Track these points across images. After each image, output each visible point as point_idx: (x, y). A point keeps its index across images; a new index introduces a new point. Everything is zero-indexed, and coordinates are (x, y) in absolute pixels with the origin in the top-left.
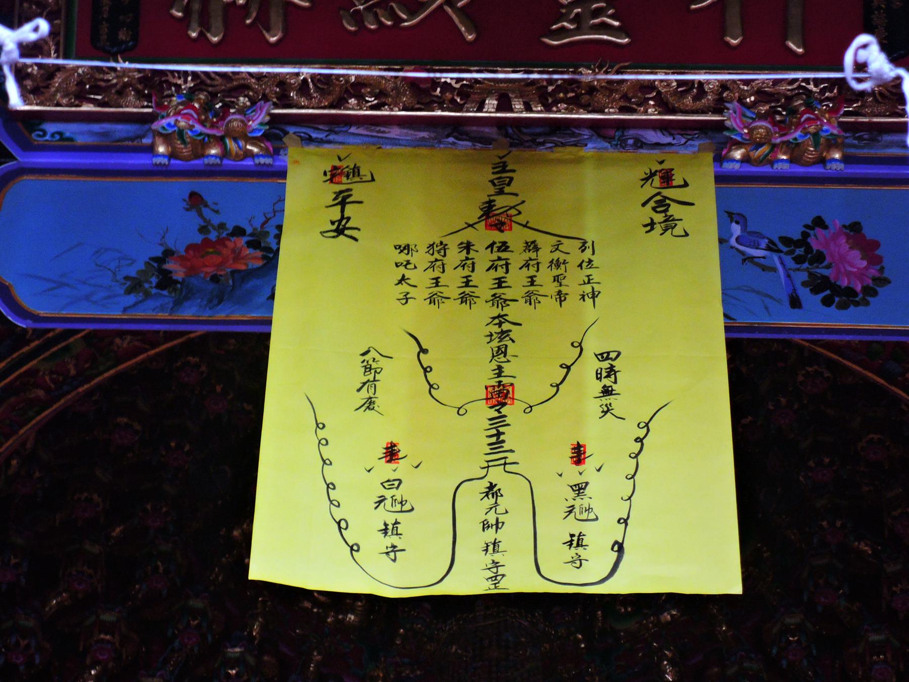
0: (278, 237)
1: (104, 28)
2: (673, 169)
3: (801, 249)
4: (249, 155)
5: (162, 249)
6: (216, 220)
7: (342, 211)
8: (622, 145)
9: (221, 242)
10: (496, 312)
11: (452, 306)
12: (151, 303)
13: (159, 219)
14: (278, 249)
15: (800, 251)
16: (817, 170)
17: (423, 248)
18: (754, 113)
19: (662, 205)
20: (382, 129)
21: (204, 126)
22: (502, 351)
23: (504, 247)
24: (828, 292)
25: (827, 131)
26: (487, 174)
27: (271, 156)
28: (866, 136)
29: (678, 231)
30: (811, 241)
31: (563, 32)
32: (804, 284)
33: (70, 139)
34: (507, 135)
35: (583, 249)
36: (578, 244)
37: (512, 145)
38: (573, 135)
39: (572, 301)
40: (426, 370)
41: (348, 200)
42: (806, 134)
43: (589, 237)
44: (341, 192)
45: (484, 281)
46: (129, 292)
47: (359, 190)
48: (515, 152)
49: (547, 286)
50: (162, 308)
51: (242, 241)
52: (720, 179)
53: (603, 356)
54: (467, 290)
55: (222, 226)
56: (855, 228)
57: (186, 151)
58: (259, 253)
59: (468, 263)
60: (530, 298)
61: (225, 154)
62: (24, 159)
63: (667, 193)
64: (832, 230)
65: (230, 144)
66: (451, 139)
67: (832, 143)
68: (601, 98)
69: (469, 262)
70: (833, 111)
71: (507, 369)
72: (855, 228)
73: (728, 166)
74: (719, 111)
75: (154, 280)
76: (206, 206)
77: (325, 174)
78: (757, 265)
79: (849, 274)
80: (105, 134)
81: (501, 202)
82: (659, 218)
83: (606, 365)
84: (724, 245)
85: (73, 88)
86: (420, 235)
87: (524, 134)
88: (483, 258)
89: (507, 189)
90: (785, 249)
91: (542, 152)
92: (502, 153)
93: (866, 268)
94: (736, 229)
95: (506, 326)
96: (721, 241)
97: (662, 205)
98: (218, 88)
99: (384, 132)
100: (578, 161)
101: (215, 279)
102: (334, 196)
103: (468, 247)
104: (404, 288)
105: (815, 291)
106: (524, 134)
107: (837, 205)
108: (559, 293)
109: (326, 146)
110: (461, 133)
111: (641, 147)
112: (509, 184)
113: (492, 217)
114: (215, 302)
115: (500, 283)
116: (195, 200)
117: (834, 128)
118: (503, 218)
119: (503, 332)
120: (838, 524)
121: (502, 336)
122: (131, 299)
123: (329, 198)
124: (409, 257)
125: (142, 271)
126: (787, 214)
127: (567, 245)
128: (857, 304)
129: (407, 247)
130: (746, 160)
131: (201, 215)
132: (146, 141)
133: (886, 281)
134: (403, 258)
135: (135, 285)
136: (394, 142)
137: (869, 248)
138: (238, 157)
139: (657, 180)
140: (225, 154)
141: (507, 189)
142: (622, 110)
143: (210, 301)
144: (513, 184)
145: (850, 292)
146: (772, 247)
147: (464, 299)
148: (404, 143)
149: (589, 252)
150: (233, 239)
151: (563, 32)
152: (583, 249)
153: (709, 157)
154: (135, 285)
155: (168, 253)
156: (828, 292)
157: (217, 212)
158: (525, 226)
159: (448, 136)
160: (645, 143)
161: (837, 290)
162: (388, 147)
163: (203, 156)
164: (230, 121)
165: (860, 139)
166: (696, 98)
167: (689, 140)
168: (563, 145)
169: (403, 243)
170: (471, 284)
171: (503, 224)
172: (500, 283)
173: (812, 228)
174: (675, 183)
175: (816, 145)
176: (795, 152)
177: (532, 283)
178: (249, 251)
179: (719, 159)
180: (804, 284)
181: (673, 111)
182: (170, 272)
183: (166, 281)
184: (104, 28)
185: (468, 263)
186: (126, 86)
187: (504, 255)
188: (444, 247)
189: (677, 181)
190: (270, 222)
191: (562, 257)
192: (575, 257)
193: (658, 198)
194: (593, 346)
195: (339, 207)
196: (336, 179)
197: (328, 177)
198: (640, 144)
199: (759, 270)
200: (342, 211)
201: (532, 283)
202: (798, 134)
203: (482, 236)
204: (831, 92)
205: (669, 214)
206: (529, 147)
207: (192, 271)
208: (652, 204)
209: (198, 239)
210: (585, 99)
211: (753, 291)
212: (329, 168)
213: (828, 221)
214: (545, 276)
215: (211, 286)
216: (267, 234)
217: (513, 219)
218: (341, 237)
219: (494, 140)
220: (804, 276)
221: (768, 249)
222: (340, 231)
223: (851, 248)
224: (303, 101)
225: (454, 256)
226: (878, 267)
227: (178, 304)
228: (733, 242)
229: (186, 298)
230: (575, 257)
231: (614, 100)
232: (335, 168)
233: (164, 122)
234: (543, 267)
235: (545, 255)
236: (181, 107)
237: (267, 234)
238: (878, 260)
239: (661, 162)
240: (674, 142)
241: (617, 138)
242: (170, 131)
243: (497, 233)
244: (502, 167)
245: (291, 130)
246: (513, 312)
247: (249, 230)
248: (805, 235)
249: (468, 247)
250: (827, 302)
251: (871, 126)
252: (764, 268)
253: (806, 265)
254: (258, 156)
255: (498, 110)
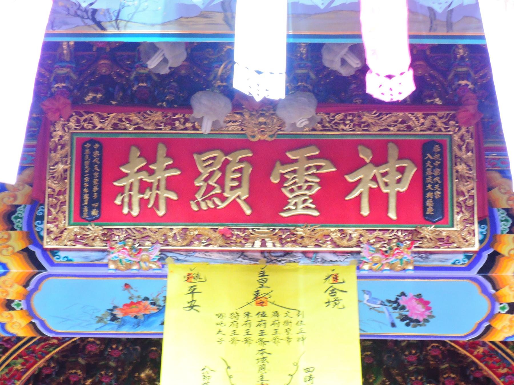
0: (165, 301)
1: (86, 209)
2: (337, 274)
3: (396, 305)
4: (150, 268)
5: (113, 306)
6: (136, 294)
7: (193, 297)
8: (316, 261)
9: (139, 303)
10: (261, 347)
11: (242, 344)
12: (107, 327)
13: (111, 293)
14: (164, 306)
15: (395, 305)
16: (402, 274)
17: (228, 315)
18: (373, 248)
19: (333, 292)
20: (210, 254)
21: (131, 257)
22: (263, 368)
23: (264, 314)
24: (408, 321)
25: (405, 258)
26: (256, 277)
27: (160, 270)
28: (424, 256)
29: (340, 306)
30: (399, 301)
31: (289, 210)
32: (398, 318)
33: (71, 260)
34: (265, 257)
35: (298, 315)
36: (296, 312)
37: (267, 262)
38: (294, 256)
39: (294, 341)
40: (230, 377)
41: (195, 291)
42: (397, 259)
43: (300, 309)
44: (192, 287)
45: (255, 331)
46: (99, 322)
47: (200, 287)
48: (269, 266)
49: (283, 335)
50: (112, 329)
51: (148, 303)
52: (359, 277)
53: (308, 370)
54: (248, 336)
55: (139, 297)
56: (419, 296)
57: (123, 267)
58: (155, 307)
59: (248, 323)
60: (275, 340)
61: (140, 268)
62: (51, 270)
63: (336, 286)
64: (409, 297)
65: (142, 264)
66: (240, 259)
67: (408, 263)
68: (306, 241)
69: (249, 322)
70: (409, 248)
71: (265, 377)
72: (419, 296)
73: (362, 273)
74: (358, 246)
75: (109, 318)
76: (132, 289)
77: (185, 277)
78: (376, 310)
79: (416, 314)
80: (86, 258)
81: (262, 291)
82: (332, 299)
83: (309, 374)
84: (361, 303)
85: (72, 237)
86: (227, 309)
87: (272, 256)
88: (255, 320)
89: (265, 285)
90: (389, 304)
91: (280, 265)
92: (263, 266)
93: (424, 312)
94: (367, 297)
95: (265, 355)
96: (360, 301)
97: (333, 292)
98: (137, 237)
99: (210, 256)
100: (296, 270)
101: (136, 317)
102: (189, 289)
103: (248, 314)
104: (220, 335)
105: (403, 320)
106: (272, 256)
107: (411, 288)
108: (288, 338)
109: (185, 263)
110: (246, 256)
111: (324, 263)
112: (265, 282)
113: (259, 299)
114: (136, 326)
115: (262, 333)
116: (127, 286)
117: (409, 256)
118: (263, 300)
119: (264, 358)
120: (420, 378)
121: (263, 357)
122: (99, 325)
123: (187, 290)
124: (221, 320)
125: (80, 5)
126: (390, 290)
127: (292, 313)
128: (421, 325)
129: (221, 315)
130: (371, 269)
131: (129, 292)
132: (105, 261)
133: (433, 317)
134: (219, 320)
135: (101, 320)
136: (215, 261)
137: (426, 304)
138: (146, 270)
139: (331, 280)
140: (140, 268)
141: (265, 285)
142: (317, 246)
143: (134, 326)
144: (268, 282)
145: (418, 321)
146: (382, 304)
147: (247, 341)
148: (219, 261)
149: (301, 316)
150: (144, 302)
151: (289, 210)
152: (298, 315)
153: (354, 267)
154: (101, 320)
155: (115, 307)
156: (408, 321)
157: (136, 291)
158: (273, 303)
159: (239, 257)
160: (326, 261)
161: (412, 321)
162: (213, 263)
163: (130, 269)
164: (142, 255)
165: (421, 257)
166: (349, 240)
167: (346, 258)
168: (290, 262)
169: (219, 313)
170: (249, 333)
171: (263, 302)
172: (262, 333)
173: (400, 296)
174: (339, 281)
175: (401, 264)
176: (392, 268)
177: (276, 333)
178: (152, 306)
179: (358, 268)
180: (398, 318)
181: (338, 246)
182: (115, 315)
183: (114, 318)
184: (86, 209)
185: (248, 323)
186: (96, 236)
187: (264, 319)
188: (237, 314)
189: (340, 280)
190: (160, 295)
191: (290, 319)
192: (295, 319)
193: (331, 289)
194: (303, 365)
195: (191, 295)
196: (190, 280)
197: (186, 279)
198: (324, 261)
199: (377, 312)
200: (193, 297)
201: (276, 333)
202: (394, 259)
203: (255, 309)
204: (408, 237)
205: (336, 297)
206: (274, 263)
207: (126, 314)
208: (329, 292)
209: (128, 302)
210: (299, 241)
211: (376, 321)
212: (186, 275)
213: (407, 294)
214: (282, 329)
215: (135, 320)
216: (158, 300)
217: (268, 300)
218: (192, 310)
219: (259, 260)
220: (397, 315)
221: (381, 304)
222: (191, 307)
223: (428, 207)
224: (174, 243)
225: (242, 319)
226: (430, 311)
227: (119, 327)
228: (365, 302)
229: (123, 325)
230: (295, 319)
231: (312, 242)
232: (189, 274)
233: (113, 256)
234: (281, 324)
235: (282, 319)
236: (121, 249)
237: (158, 300)
238: (429, 309)
239: (333, 270)
240: (339, 260)
241: (314, 258)
242: (116, 259)
243: (260, 307)
244: (263, 274)
245: (169, 254)
246: (268, 347)
247: (151, 298)
248: (397, 299)
249: (248, 314)
250: (408, 325)
251: (425, 252)
252: (379, 312)
253: (398, 311)
254: (154, 269)
255: (261, 246)
